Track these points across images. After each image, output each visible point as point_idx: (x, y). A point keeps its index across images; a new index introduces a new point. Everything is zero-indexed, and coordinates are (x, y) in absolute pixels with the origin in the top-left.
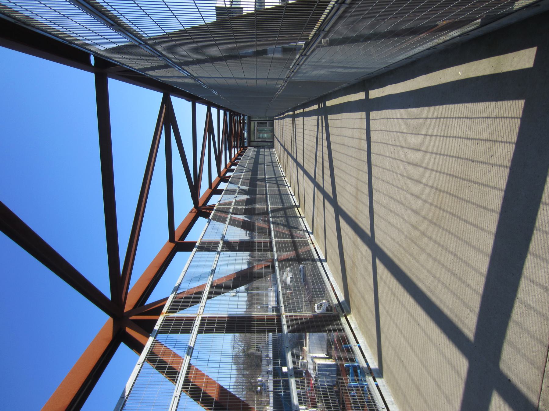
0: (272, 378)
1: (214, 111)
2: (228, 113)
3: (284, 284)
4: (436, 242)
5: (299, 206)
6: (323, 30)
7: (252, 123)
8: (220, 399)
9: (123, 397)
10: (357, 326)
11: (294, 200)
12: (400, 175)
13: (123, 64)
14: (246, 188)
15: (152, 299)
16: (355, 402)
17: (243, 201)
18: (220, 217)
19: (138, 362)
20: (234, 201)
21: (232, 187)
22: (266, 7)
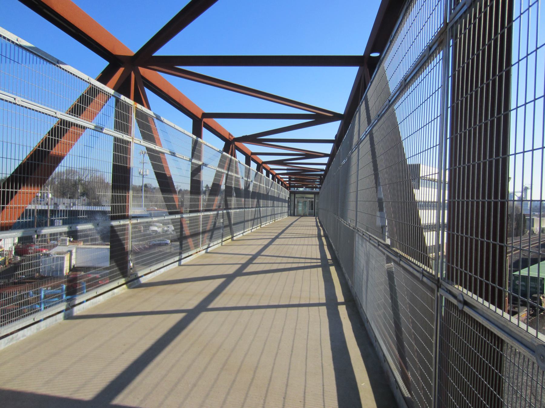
0: (50, 208)
1: (325, 160)
2: (323, 173)
3: (149, 224)
4: (206, 368)
5: (233, 240)
6: (400, 260)
7: (312, 196)
8: (51, 156)
9: (58, 62)
10: (116, 295)
11: (238, 235)
12: (269, 335)
13: (371, 83)
14: (251, 189)
15: (150, 95)
16: (22, 297)
17: (239, 185)
18: (225, 163)
19: (90, 78)
20: (239, 176)
21: (252, 175)
22: (420, 211)
